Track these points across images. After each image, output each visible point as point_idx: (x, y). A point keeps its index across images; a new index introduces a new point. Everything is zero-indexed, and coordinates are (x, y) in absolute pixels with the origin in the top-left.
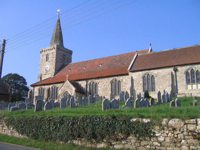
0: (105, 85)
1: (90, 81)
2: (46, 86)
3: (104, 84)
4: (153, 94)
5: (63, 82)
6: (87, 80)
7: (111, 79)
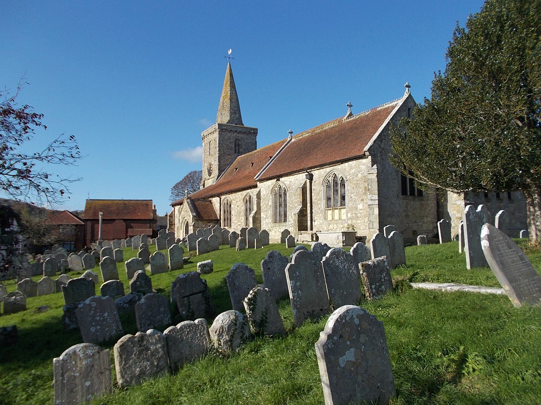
0: (238, 206)
1: (223, 197)
6: (219, 195)
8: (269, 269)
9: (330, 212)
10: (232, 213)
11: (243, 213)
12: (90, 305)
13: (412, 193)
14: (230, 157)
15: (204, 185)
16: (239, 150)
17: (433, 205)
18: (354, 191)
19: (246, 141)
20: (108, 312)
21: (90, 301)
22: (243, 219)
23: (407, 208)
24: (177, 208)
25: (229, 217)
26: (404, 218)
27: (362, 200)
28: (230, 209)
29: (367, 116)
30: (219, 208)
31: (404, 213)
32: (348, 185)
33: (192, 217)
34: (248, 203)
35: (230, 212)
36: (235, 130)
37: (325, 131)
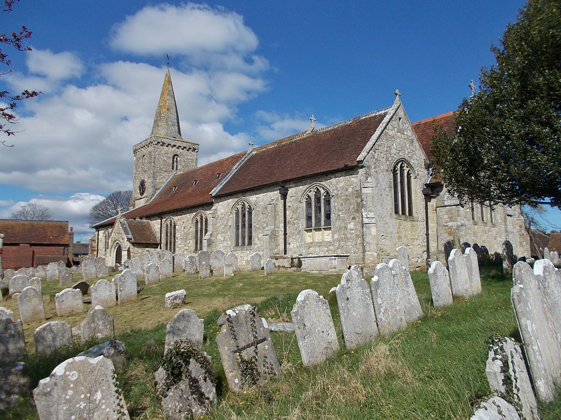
0: (184, 228)
2: (334, 180)
3: (184, 226)
4: (248, 252)
6: (160, 215)
8: (348, 299)
10: (177, 236)
11: (192, 235)
12: (64, 376)
13: (404, 213)
14: (166, 174)
15: (134, 206)
16: (177, 166)
17: (422, 226)
18: (341, 208)
19: (186, 157)
20: (102, 391)
21: (66, 369)
22: (192, 243)
23: (400, 229)
24: (101, 232)
25: (173, 240)
26: (397, 240)
27: (354, 218)
28: (175, 231)
29: (349, 125)
30: (159, 230)
31: (397, 235)
32: (335, 202)
33: (126, 239)
34: (199, 224)
35: (175, 234)
36: (174, 144)
37: (295, 142)
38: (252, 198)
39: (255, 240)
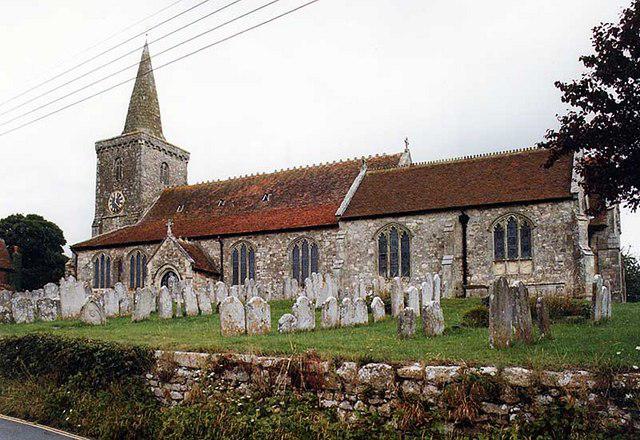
5: (159, 242)
7: (292, 237)
9: (499, 265)
38: (412, 223)
39: (535, 250)
